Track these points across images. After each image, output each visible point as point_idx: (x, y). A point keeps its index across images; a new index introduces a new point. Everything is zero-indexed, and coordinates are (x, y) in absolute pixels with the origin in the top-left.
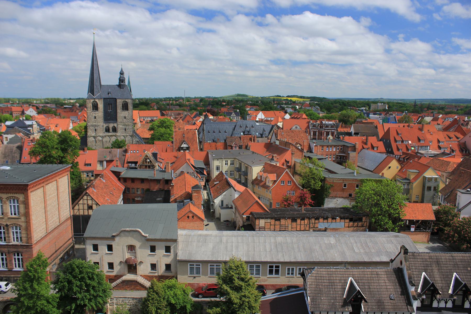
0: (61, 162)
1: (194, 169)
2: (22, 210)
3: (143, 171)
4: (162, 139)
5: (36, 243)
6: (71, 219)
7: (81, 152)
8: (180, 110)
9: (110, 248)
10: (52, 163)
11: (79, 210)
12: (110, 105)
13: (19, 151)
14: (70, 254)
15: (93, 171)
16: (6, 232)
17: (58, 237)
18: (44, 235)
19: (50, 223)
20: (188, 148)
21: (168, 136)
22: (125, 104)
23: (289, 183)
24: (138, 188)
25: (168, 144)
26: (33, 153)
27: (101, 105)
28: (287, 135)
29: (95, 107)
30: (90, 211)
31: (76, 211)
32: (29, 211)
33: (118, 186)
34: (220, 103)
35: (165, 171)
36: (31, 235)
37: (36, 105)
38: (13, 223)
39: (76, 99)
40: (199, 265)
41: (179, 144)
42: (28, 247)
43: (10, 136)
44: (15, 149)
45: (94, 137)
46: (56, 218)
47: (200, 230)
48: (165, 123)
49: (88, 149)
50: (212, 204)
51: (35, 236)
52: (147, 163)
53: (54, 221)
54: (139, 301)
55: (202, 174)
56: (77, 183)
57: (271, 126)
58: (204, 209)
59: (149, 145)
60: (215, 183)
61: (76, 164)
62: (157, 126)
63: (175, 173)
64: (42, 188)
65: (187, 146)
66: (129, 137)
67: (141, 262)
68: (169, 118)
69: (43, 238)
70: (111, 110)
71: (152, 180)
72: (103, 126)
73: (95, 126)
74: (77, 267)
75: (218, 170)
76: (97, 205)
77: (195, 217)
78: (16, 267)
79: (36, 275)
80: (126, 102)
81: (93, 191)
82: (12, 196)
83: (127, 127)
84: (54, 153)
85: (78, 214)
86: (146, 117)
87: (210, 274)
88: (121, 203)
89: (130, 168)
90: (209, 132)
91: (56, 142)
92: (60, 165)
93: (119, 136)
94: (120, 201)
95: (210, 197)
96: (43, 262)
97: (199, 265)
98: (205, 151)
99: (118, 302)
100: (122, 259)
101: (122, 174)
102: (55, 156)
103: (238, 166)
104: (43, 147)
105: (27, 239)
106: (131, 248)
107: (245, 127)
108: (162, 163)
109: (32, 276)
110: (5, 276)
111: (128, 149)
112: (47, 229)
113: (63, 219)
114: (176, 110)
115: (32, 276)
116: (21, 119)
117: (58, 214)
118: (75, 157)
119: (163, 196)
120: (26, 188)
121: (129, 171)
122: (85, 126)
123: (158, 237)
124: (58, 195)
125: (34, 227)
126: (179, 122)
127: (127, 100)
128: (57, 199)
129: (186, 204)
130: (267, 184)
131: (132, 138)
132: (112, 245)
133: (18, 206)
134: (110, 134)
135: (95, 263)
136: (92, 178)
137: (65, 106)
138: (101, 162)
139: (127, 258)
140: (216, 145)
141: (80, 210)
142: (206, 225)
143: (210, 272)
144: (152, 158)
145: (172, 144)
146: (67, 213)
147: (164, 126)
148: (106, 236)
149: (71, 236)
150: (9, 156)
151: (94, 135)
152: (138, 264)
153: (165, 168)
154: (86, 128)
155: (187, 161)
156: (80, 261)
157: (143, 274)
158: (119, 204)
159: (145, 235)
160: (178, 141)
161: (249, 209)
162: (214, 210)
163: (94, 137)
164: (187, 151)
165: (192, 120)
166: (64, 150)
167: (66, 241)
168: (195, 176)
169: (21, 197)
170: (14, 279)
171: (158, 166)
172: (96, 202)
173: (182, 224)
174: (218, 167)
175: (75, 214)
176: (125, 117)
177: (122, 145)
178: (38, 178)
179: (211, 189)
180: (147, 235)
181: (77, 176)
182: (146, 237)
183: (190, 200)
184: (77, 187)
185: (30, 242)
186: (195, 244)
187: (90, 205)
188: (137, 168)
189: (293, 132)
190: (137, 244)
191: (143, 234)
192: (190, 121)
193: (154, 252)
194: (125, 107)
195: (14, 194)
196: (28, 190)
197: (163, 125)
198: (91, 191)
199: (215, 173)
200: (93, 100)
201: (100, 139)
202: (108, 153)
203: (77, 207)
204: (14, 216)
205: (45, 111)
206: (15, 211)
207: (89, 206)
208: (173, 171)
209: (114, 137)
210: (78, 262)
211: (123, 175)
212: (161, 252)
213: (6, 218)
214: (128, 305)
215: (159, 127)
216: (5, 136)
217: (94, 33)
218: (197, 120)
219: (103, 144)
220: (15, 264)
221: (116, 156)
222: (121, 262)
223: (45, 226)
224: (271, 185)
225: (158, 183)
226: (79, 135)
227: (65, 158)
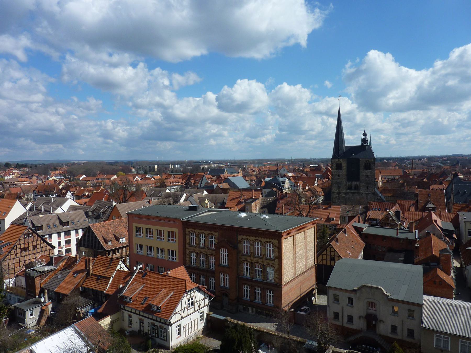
2: (187, 238)
5: (285, 285)
27: (344, 165)
45: (339, 193)
46: (302, 265)
51: (285, 278)
53: (300, 267)
82: (192, 230)
85: (321, 263)
94: (361, 257)
101: (364, 230)
134: (353, 191)
141: (323, 260)
146: (312, 262)
159: (387, 294)
169: (276, 242)
187: (333, 256)
191: (385, 293)
200: (338, 160)
201: (343, 195)
203: (320, 257)
208: (417, 231)
216: (264, 190)
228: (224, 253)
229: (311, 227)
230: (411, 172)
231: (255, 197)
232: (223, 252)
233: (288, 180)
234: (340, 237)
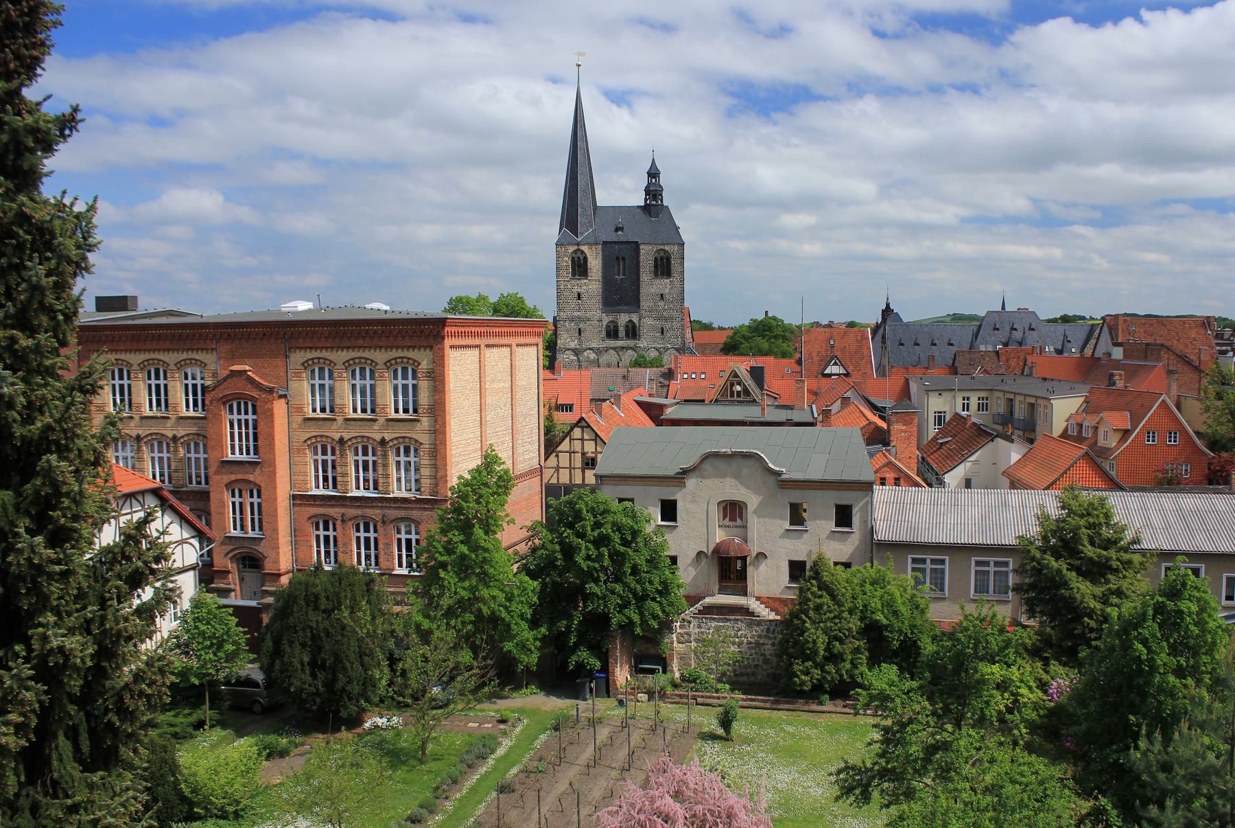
2: (424, 398)
11: (558, 468)
16: (380, 461)
23: (1170, 437)
27: (595, 263)
28: (1145, 332)
36: (446, 470)
38: (398, 435)
40: (942, 562)
45: (576, 352)
54: (768, 630)
57: (1087, 329)
65: (842, 371)
67: (761, 556)
72: (600, 321)
74: (592, 510)
77: (902, 481)
78: (400, 565)
83: (667, 325)
85: (554, 481)
87: (976, 592)
90: (903, 344)
97: (942, 562)
99: (702, 633)
100: (705, 545)
103: (1002, 410)
105: (433, 481)
106: (733, 510)
107: (1008, 329)
111: (676, 367)
121: (685, 407)
123: (815, 474)
125: (454, 452)
127: (667, 248)
128: (509, 400)
130: (1099, 444)
133: (414, 386)
134: (620, 343)
139: (718, 541)
141: (561, 470)
143: (976, 585)
144: (750, 383)
145: (798, 368)
151: (573, 345)
152: (752, 563)
157: (764, 594)
160: (815, 359)
161: (1062, 476)
163: (576, 352)
169: (424, 360)
174: (940, 417)
183: (884, 446)
187: (590, 455)
189: (1165, 325)
190: (752, 501)
191: (771, 465)
195: (324, 351)
196: (443, 338)
201: (593, 356)
202: (620, 380)
203: (552, 461)
206: (406, 403)
212: (821, 525)
214: (734, 643)
217: (579, 66)
220: (400, 557)
222: (700, 553)
224: (1114, 444)
228: (243, 417)
232: (239, 413)
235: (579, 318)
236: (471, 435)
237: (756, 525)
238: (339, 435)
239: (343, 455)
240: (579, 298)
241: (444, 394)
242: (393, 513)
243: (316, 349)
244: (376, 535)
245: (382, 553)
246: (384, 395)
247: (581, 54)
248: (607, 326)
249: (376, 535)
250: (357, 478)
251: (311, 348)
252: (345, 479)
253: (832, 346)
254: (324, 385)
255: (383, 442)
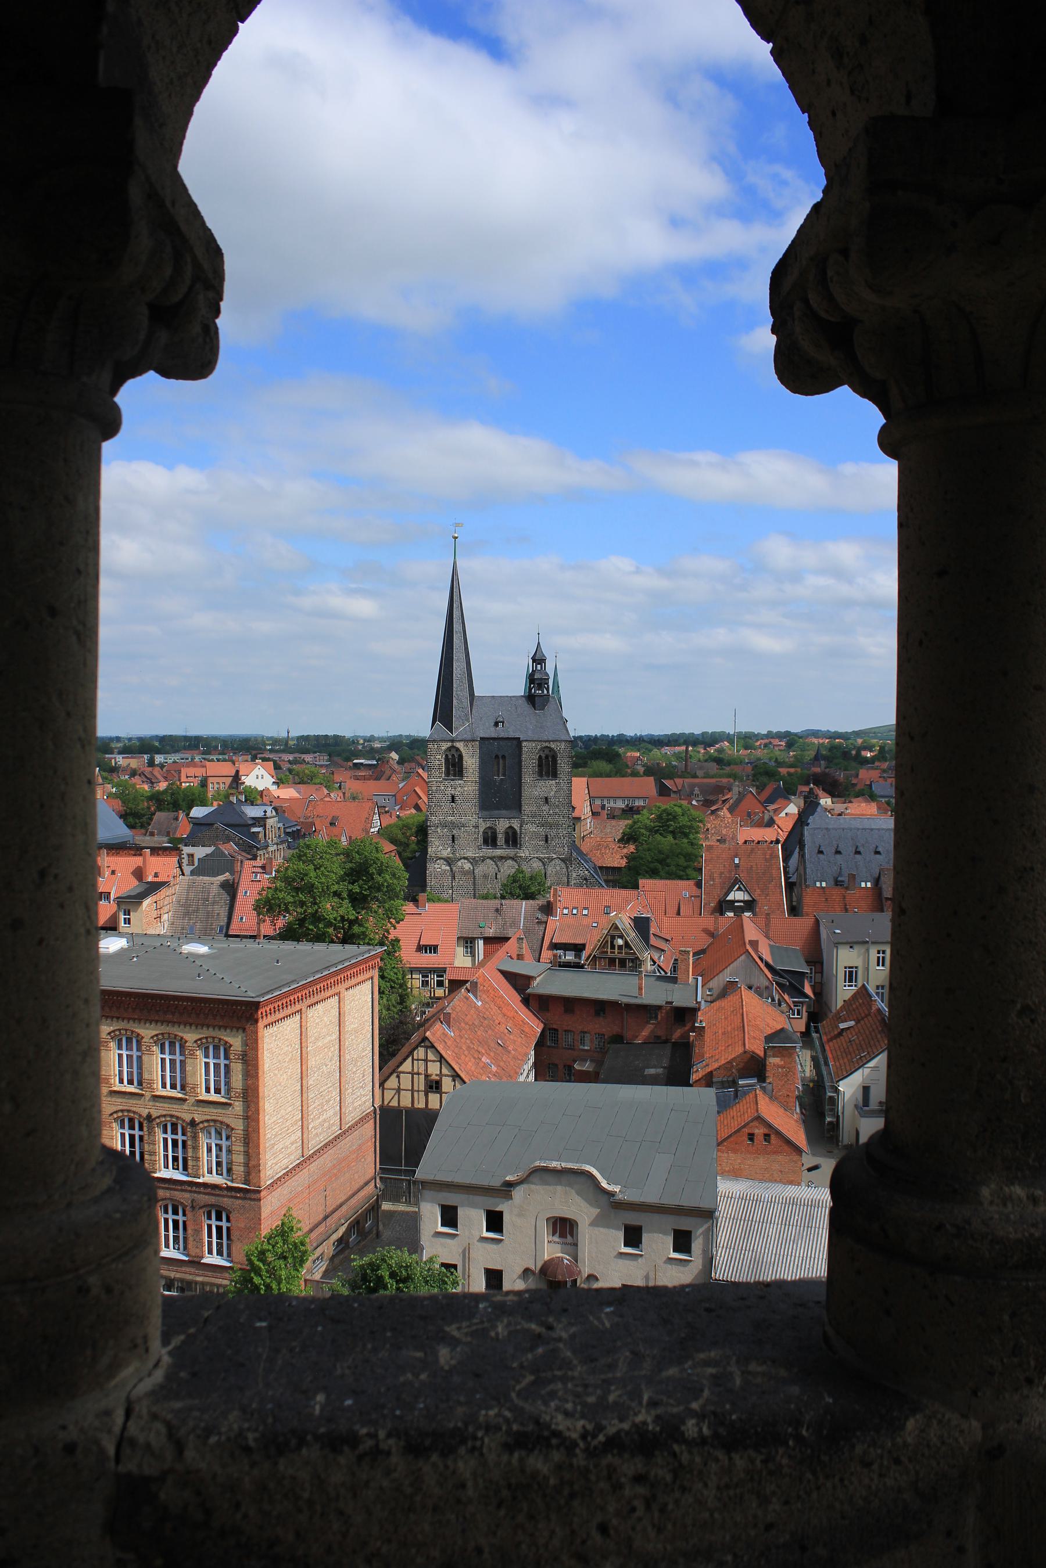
0: (347, 939)
1: (770, 976)
2: (237, 1080)
3: (604, 976)
4: (662, 873)
5: (272, 1185)
6: (375, 1118)
7: (409, 907)
8: (721, 776)
9: (495, 1221)
10: (319, 938)
11: (399, 1090)
12: (501, 761)
13: (226, 897)
14: (367, 1230)
15: (444, 970)
16: (189, 1143)
17: (335, 1171)
18: (295, 1164)
19: (315, 1128)
20: (750, 905)
21: (682, 861)
22: (547, 757)
24: (586, 1030)
25: (684, 888)
26: (267, 906)
27: (471, 762)
29: (455, 766)
30: (434, 1100)
31: (389, 1095)
32: (258, 1086)
33: (523, 1020)
34: (854, 752)
35: (673, 980)
36: (259, 1160)
37: (271, 756)
38: (209, 1118)
39: (389, 738)
41: (722, 889)
42: (248, 1196)
43: (200, 852)
44: (215, 889)
45: (449, 861)
46: (331, 1113)
47: (791, 1183)
48: (675, 818)
49: (429, 900)
50: (830, 1097)
51: (270, 1164)
52: (616, 951)
53: (325, 1121)
55: (796, 990)
56: (394, 1006)
58: (802, 1113)
59: (624, 893)
60: (842, 1026)
61: (393, 945)
62: (646, 828)
63: (707, 986)
64: (298, 1017)
65: (747, 898)
66: (558, 862)
68: (684, 803)
69: (290, 1171)
70: (504, 775)
71: (630, 1008)
72: (476, 827)
73: (453, 825)
75: (850, 981)
76: (454, 1080)
77: (773, 1137)
78: (210, 1252)
79: (274, 1286)
80: (551, 749)
81: (445, 1035)
83: (552, 833)
84: (328, 907)
85: (394, 1103)
86: (609, 798)
88: (528, 1076)
89: (560, 966)
91: (336, 874)
92: (351, 949)
93: (527, 860)
94: (526, 1073)
95: (825, 1073)
96: (295, 1245)
98: (807, 915)
101: (535, 983)
102: (331, 916)
104: (297, 890)
106: (564, 1227)
108: (663, 950)
109: (262, 1287)
110: (178, 1275)
112: (305, 1146)
113: (350, 1118)
114: (707, 776)
115: (262, 1287)
116: (234, 799)
117: (338, 1098)
118: (391, 923)
119: (665, 1063)
120: (252, 1013)
121: (557, 973)
122: (421, 826)
124: (342, 1040)
125: (269, 1136)
126: (718, 816)
129: (745, 1093)
131: (567, 868)
132: (500, 1214)
134: (498, 852)
135: (443, 1265)
136: (440, 992)
137: (355, 761)
138: (468, 942)
139: (546, 1258)
140: (844, 897)
141: (402, 1093)
142: (810, 1170)
144: (632, 935)
145: (695, 891)
146: (364, 1099)
147: (671, 829)
148: (485, 1182)
149: (370, 1172)
150: (197, 910)
151: (446, 853)
153: (675, 969)
154: (422, 831)
155: (748, 947)
156: (406, 1257)
158: (522, 1079)
162: (838, 1117)
163: (449, 861)
164: (747, 914)
165: (763, 809)
166: (358, 901)
167: (357, 1186)
168: (773, 1000)
169: (236, 1042)
170: (203, 1289)
171: (649, 963)
172: (453, 1069)
173: (732, 1159)
174: (851, 973)
175: (386, 1103)
176: (546, 798)
177: (533, 889)
178: (288, 984)
179: (827, 1047)
180: (616, 1189)
181: (394, 982)
182: (613, 1195)
184: (393, 1018)
185: (255, 1181)
186: (773, 1231)
187: (434, 1077)
188: (582, 967)
191: (604, 1184)
192: (756, 814)
193: (638, 1247)
194: (548, 766)
195: (131, 1022)
196: (256, 1021)
197: (668, 826)
198: (439, 1033)
199: (843, 992)
201: (467, 866)
202: (492, 914)
203: (392, 1083)
204: (213, 1097)
205: (298, 775)
207: (432, 1081)
209: (510, 862)
210: (398, 1256)
211: (538, 987)
213: (191, 1100)
215: (653, 831)
216: (187, 850)
218: (777, 811)
219: (474, 884)
220: (210, 1243)
221: (515, 924)
223: (299, 1134)
225: (651, 1018)
226: (400, 854)
227: (361, 925)
229: (361, 978)
230: (683, 786)
231: (156, 875)
233: (274, 813)
234: (458, 1009)
235: (452, 823)
236: (290, 1109)
237: (586, 1234)
238: (147, 1111)
239: (151, 1132)
240: (453, 801)
241: (258, 1080)
242: (204, 1199)
243: (208, 1027)
244: (185, 1219)
245: (191, 1239)
246: (194, 1073)
247: (457, 525)
248: (484, 832)
249: (185, 1219)
250: (166, 1157)
251: (118, 1018)
252: (153, 1158)
253: (737, 866)
254: (131, 1056)
255: (193, 1123)
